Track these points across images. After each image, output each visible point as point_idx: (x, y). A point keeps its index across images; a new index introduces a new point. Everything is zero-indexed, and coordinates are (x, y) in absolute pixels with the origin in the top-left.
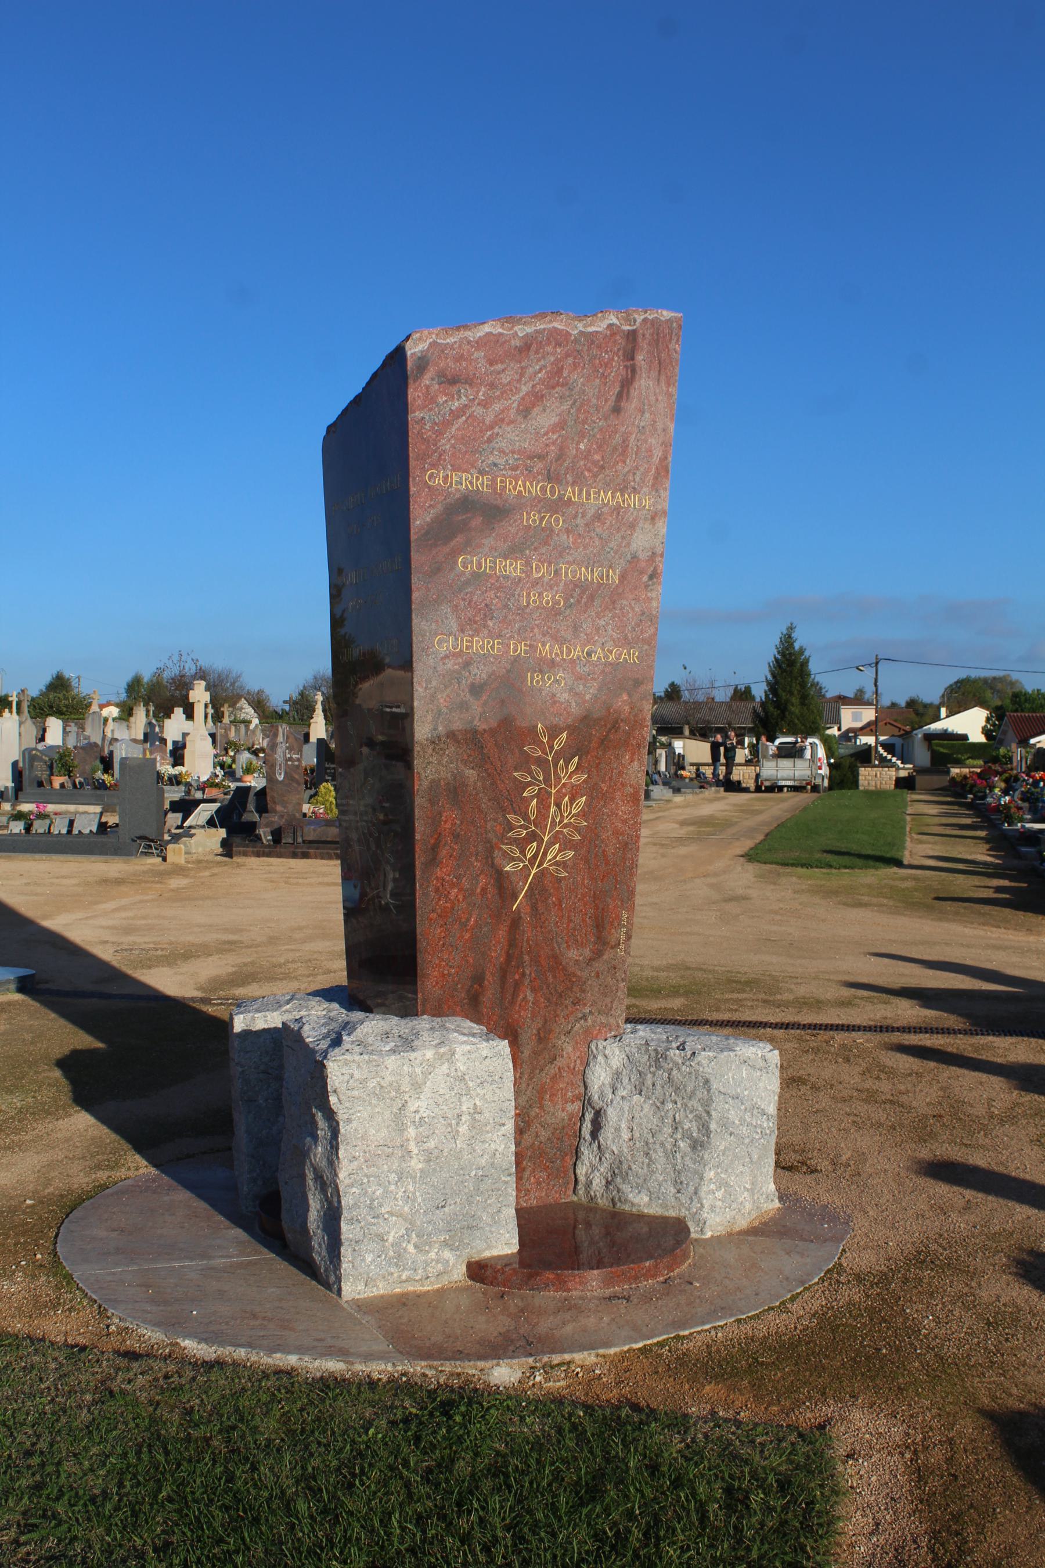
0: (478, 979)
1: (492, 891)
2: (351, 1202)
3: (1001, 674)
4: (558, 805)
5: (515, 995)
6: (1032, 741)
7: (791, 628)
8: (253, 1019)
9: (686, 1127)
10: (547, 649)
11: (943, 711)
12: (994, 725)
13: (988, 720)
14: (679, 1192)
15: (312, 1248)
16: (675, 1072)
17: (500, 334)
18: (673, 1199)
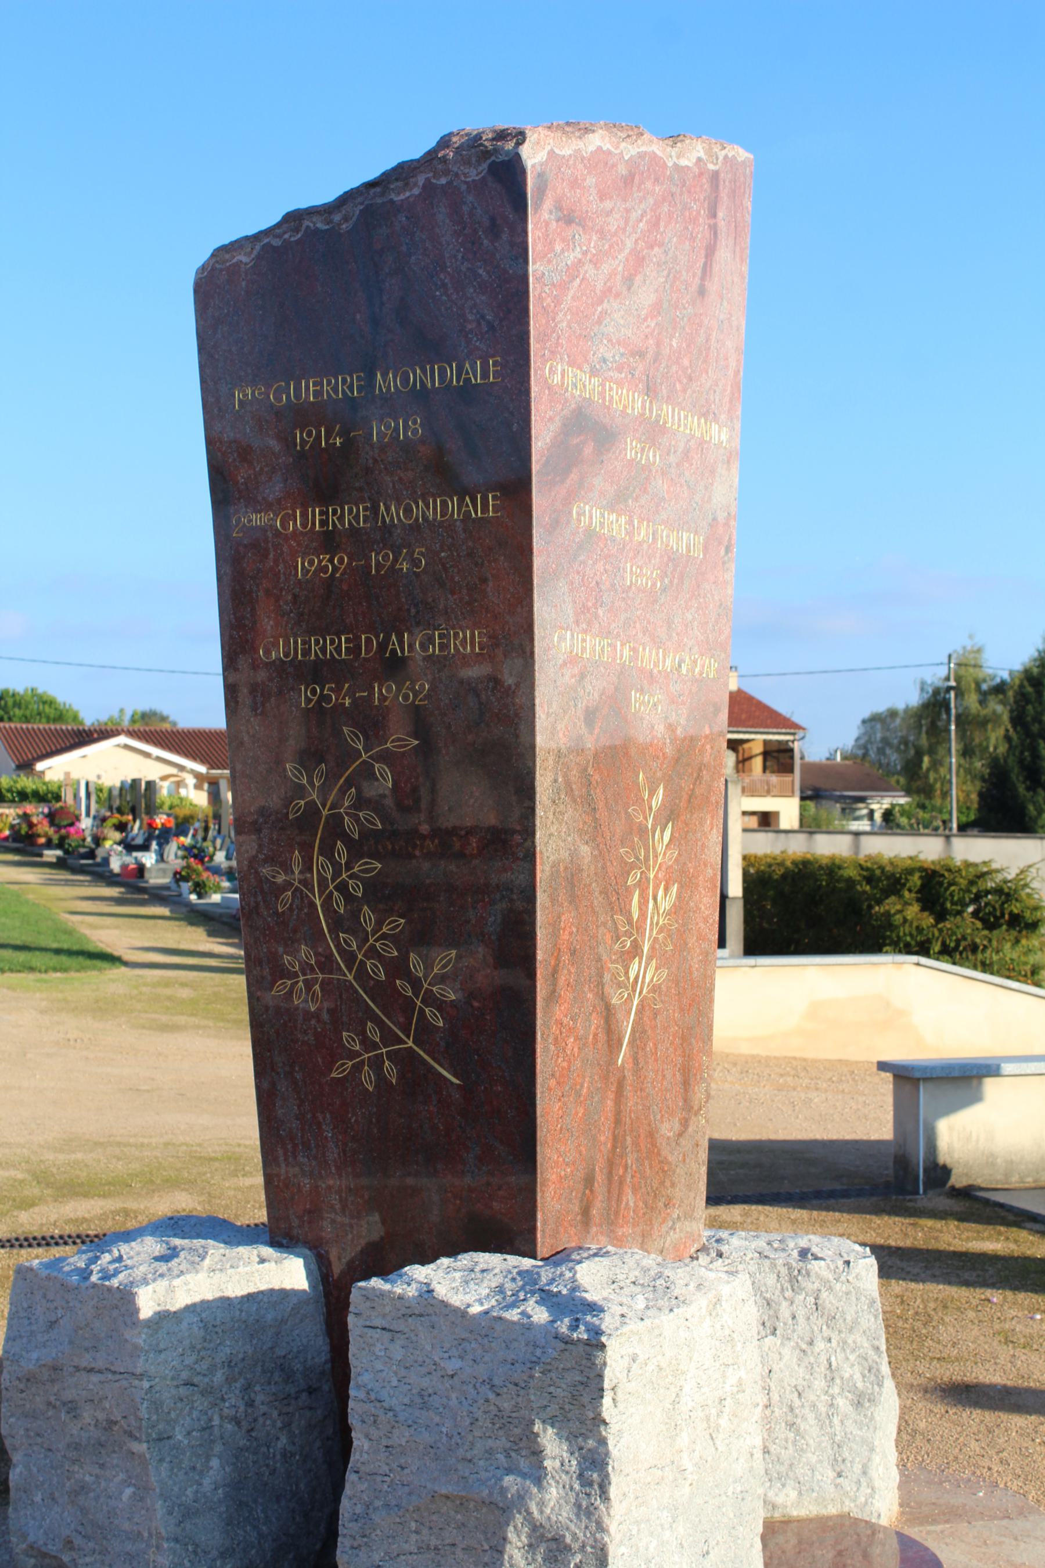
0: (589, 1181)
1: (602, 1037)
4: (655, 899)
5: (619, 1200)
6: (40, 766)
8: (171, 1290)
9: (846, 1375)
10: (648, 657)
14: (839, 1475)
16: (824, 1294)
17: (609, 152)
18: (832, 1489)
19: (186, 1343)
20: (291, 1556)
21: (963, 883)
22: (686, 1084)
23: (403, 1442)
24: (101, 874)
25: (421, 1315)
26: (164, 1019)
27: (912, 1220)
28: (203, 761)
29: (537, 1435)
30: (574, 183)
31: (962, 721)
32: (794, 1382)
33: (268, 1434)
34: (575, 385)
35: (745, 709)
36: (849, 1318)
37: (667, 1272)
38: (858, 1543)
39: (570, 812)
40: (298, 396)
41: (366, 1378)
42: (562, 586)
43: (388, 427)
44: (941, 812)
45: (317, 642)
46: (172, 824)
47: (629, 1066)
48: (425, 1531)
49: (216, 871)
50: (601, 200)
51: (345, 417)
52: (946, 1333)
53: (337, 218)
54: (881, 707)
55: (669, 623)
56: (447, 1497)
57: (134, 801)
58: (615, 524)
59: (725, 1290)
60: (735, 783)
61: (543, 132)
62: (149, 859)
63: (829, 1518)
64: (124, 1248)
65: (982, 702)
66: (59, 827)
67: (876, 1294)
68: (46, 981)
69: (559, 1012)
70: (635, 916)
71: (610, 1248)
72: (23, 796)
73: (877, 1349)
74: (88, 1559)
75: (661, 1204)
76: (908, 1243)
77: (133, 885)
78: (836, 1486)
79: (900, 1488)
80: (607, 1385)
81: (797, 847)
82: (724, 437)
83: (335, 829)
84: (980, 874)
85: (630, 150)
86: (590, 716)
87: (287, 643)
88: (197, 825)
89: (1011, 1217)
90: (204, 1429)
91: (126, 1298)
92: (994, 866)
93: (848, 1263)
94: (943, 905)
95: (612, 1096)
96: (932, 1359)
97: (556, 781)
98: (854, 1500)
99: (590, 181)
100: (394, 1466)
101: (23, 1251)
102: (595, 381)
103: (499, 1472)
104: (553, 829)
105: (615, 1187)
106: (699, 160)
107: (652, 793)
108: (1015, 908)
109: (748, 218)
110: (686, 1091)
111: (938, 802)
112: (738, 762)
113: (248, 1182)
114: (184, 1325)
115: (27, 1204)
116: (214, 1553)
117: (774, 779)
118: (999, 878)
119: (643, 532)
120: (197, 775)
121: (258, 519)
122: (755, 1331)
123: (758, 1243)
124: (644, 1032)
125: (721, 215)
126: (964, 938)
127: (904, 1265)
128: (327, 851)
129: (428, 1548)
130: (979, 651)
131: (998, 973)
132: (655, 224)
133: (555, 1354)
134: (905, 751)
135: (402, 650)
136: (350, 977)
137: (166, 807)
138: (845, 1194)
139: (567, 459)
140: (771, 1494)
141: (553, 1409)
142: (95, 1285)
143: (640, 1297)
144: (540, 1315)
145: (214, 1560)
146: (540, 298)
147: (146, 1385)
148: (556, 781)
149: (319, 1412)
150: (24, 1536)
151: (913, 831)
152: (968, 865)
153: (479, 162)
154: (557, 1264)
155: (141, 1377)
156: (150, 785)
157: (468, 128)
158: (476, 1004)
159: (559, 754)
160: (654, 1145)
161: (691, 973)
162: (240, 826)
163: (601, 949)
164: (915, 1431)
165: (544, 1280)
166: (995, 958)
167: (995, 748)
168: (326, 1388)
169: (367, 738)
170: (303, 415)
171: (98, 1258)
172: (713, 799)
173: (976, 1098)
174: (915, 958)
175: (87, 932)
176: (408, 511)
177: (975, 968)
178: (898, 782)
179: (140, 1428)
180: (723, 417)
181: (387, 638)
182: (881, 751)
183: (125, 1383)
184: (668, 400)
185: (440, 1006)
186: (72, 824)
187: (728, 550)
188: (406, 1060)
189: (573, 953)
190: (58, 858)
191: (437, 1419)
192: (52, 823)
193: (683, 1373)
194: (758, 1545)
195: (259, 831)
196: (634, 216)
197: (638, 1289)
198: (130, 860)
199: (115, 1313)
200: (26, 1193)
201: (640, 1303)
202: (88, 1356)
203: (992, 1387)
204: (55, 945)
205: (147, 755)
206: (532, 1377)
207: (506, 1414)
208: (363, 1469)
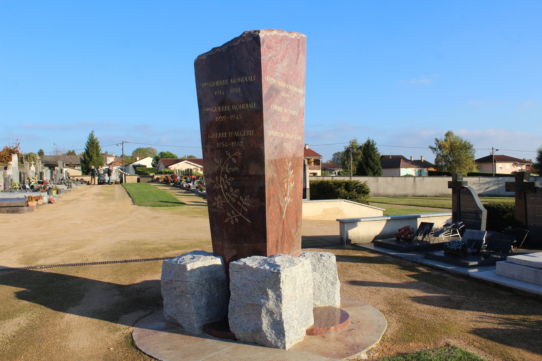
0: (277, 241)
7: (93, 132)
8: (194, 265)
10: (287, 136)
11: (138, 159)
15: (266, 337)
22: (297, 222)
24: (182, 187)
30: (270, 41)
31: (353, 154)
41: (233, 281)
42: (269, 122)
49: (204, 186)
51: (225, 88)
52: (350, 271)
54: (337, 152)
55: (292, 129)
57: (188, 173)
58: (280, 109)
59: (305, 262)
62: (191, 184)
64: (184, 257)
69: (271, 207)
72: (166, 173)
81: (321, 179)
85: (281, 34)
86: (276, 148)
91: (185, 266)
99: (273, 40)
105: (283, 243)
115: (167, 251)
117: (316, 166)
120: (201, 168)
128: (223, 176)
138: (330, 246)
139: (270, 96)
144: (268, 268)
155: (188, 282)
170: (216, 88)
173: (356, 226)
176: (238, 107)
182: (337, 160)
188: (240, 218)
201: (288, 265)
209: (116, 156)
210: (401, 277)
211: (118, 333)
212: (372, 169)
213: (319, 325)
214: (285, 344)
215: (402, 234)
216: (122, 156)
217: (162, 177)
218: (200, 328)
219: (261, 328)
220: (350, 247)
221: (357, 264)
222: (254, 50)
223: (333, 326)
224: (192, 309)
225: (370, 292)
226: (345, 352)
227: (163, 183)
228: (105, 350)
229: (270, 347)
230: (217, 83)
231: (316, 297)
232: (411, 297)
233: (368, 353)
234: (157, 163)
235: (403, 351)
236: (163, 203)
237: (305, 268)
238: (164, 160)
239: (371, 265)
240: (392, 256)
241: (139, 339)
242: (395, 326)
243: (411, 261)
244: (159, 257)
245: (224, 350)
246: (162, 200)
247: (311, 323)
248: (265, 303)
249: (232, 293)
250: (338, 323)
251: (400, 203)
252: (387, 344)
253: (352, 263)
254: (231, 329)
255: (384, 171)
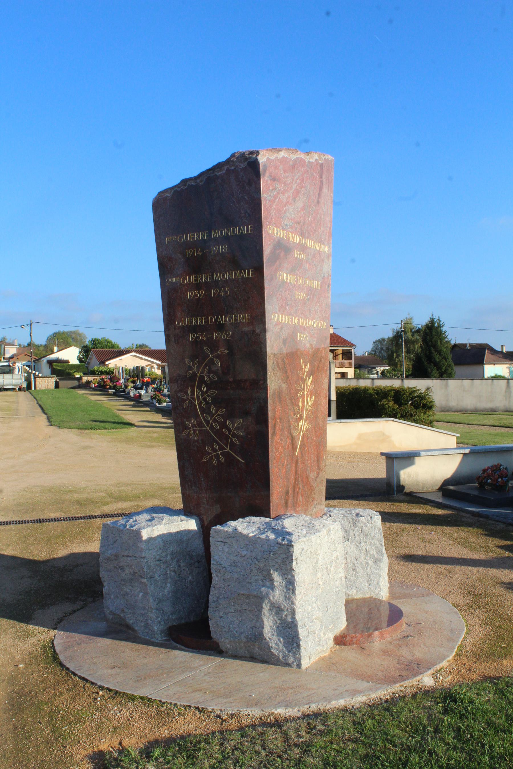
0: (287, 493)
1: (290, 446)
2: (300, 617)
3: (72, 329)
5: (297, 499)
6: (107, 363)
8: (152, 530)
10: (304, 322)
11: (56, 349)
12: (83, 355)
13: (80, 352)
14: (370, 585)
15: (269, 648)
16: (364, 528)
17: (287, 158)
18: (367, 589)
19: (158, 547)
20: (194, 614)
21: (407, 394)
22: (318, 461)
23: (229, 577)
24: (127, 397)
25: (234, 537)
26: (149, 444)
27: (392, 503)
28: (159, 360)
29: (272, 574)
30: (276, 168)
31: (407, 342)
32: (355, 556)
33: (185, 575)
34: (277, 234)
35: (335, 339)
36: (372, 535)
37: (313, 522)
38: (376, 606)
39: (279, 373)
40: (187, 239)
41: (216, 557)
42: (275, 299)
43: (216, 248)
44: (400, 371)
45: (195, 319)
46: (150, 380)
47: (299, 455)
48: (236, 605)
50: (285, 173)
51: (203, 245)
52: (403, 539)
53: (198, 181)
54: (378, 338)
55: (310, 311)
56: (243, 595)
57: (137, 373)
58: (291, 278)
59: (332, 527)
60: (333, 363)
61: (265, 152)
62: (143, 392)
63: (366, 598)
64: (137, 517)
65: (413, 336)
66: (114, 382)
67: (381, 527)
68: (110, 432)
69: (276, 438)
70: (301, 406)
71: (294, 514)
72: (102, 373)
73: (381, 545)
74: (129, 616)
75: (311, 500)
76: (391, 511)
77: (138, 401)
78: (369, 588)
79: (389, 588)
80: (294, 558)
81: (354, 384)
82: (326, 249)
83: (202, 380)
84: (412, 391)
85: (294, 157)
86: (285, 341)
87: (185, 320)
88: (158, 381)
89: (424, 502)
90: (164, 574)
91: (138, 534)
92: (417, 388)
93: (371, 517)
94: (401, 401)
95: (294, 465)
96: (399, 547)
97: (274, 363)
98: (374, 593)
100: (226, 585)
101: (105, 519)
102: (284, 232)
103: (260, 587)
104: (273, 379)
105: (296, 495)
106: (316, 160)
107: (305, 366)
108: (424, 402)
109: (333, 178)
110: (318, 463)
111: (399, 368)
112: (334, 357)
113: (177, 495)
114: (157, 542)
115: (107, 504)
116: (169, 613)
117: (346, 362)
118: (419, 392)
119: (301, 281)
120: (158, 365)
121: (175, 280)
122: (342, 540)
123: (342, 511)
124: (304, 444)
125: (324, 177)
126: (408, 412)
127: (390, 518)
129: (238, 611)
130: (411, 319)
131: (419, 423)
132: (302, 181)
133: (277, 549)
134: (388, 352)
135: (223, 321)
136: (208, 429)
137: (148, 375)
138: (370, 496)
139: (275, 257)
140: (348, 591)
141: (277, 566)
142: (128, 529)
143: (304, 530)
144: (272, 536)
145: (169, 615)
146: (265, 206)
147: (145, 561)
148: (274, 363)
149: (201, 569)
150: (109, 608)
151: (391, 378)
152: (409, 388)
153: (244, 162)
154: (277, 520)
155: (144, 558)
156: (142, 368)
157: (241, 151)
158: (249, 436)
159: (275, 354)
160: (308, 481)
161: (319, 425)
162: (171, 381)
163: (290, 418)
164: (394, 570)
165: (273, 525)
166: (418, 418)
167: (417, 350)
168: (203, 561)
169: (211, 351)
170: (189, 245)
171: (129, 521)
172: (325, 368)
173: (413, 463)
174: (392, 419)
175: (123, 416)
176: (223, 276)
177: (412, 422)
178: (386, 362)
179: (144, 574)
180: (326, 243)
181: (218, 318)
183: (139, 560)
184: (308, 238)
185: (238, 437)
186: (118, 381)
187: (329, 286)
188: (226, 455)
189: (281, 419)
190: (113, 392)
191: (239, 570)
192: (111, 381)
193: (319, 554)
194: (344, 607)
195: (177, 381)
196: (296, 178)
197: (304, 527)
198: (136, 392)
199: (135, 538)
200: (106, 500)
201: (305, 532)
202: (127, 552)
203: (418, 556)
204: (113, 421)
205: (141, 358)
206: (270, 556)
207: (262, 568)
208: (216, 586)
209: (20, 345)
210: (486, 549)
211: (31, 640)
212: (438, 366)
213: (355, 627)
214: (300, 660)
215: (488, 477)
216: (29, 345)
217: (94, 379)
218: (162, 632)
219: (261, 634)
220: (402, 497)
221: (414, 526)
222: (250, 183)
223: (376, 629)
224: (152, 601)
225: (438, 574)
226: (397, 673)
227: (97, 390)
228: (10, 668)
229: (277, 665)
230: (190, 237)
231: (349, 583)
232: (504, 583)
233: (435, 675)
234: (87, 356)
235: (493, 673)
236: (98, 423)
237: (333, 536)
238: (97, 351)
239: (439, 528)
240: (473, 513)
241: (66, 649)
242: (480, 631)
243: (504, 523)
244: (94, 514)
245: (202, 668)
246: (97, 418)
247: (342, 625)
248: (267, 594)
249: (214, 576)
250: (385, 624)
251: (485, 422)
252: (465, 660)
253: (406, 525)
254: (213, 635)
255: (458, 370)
